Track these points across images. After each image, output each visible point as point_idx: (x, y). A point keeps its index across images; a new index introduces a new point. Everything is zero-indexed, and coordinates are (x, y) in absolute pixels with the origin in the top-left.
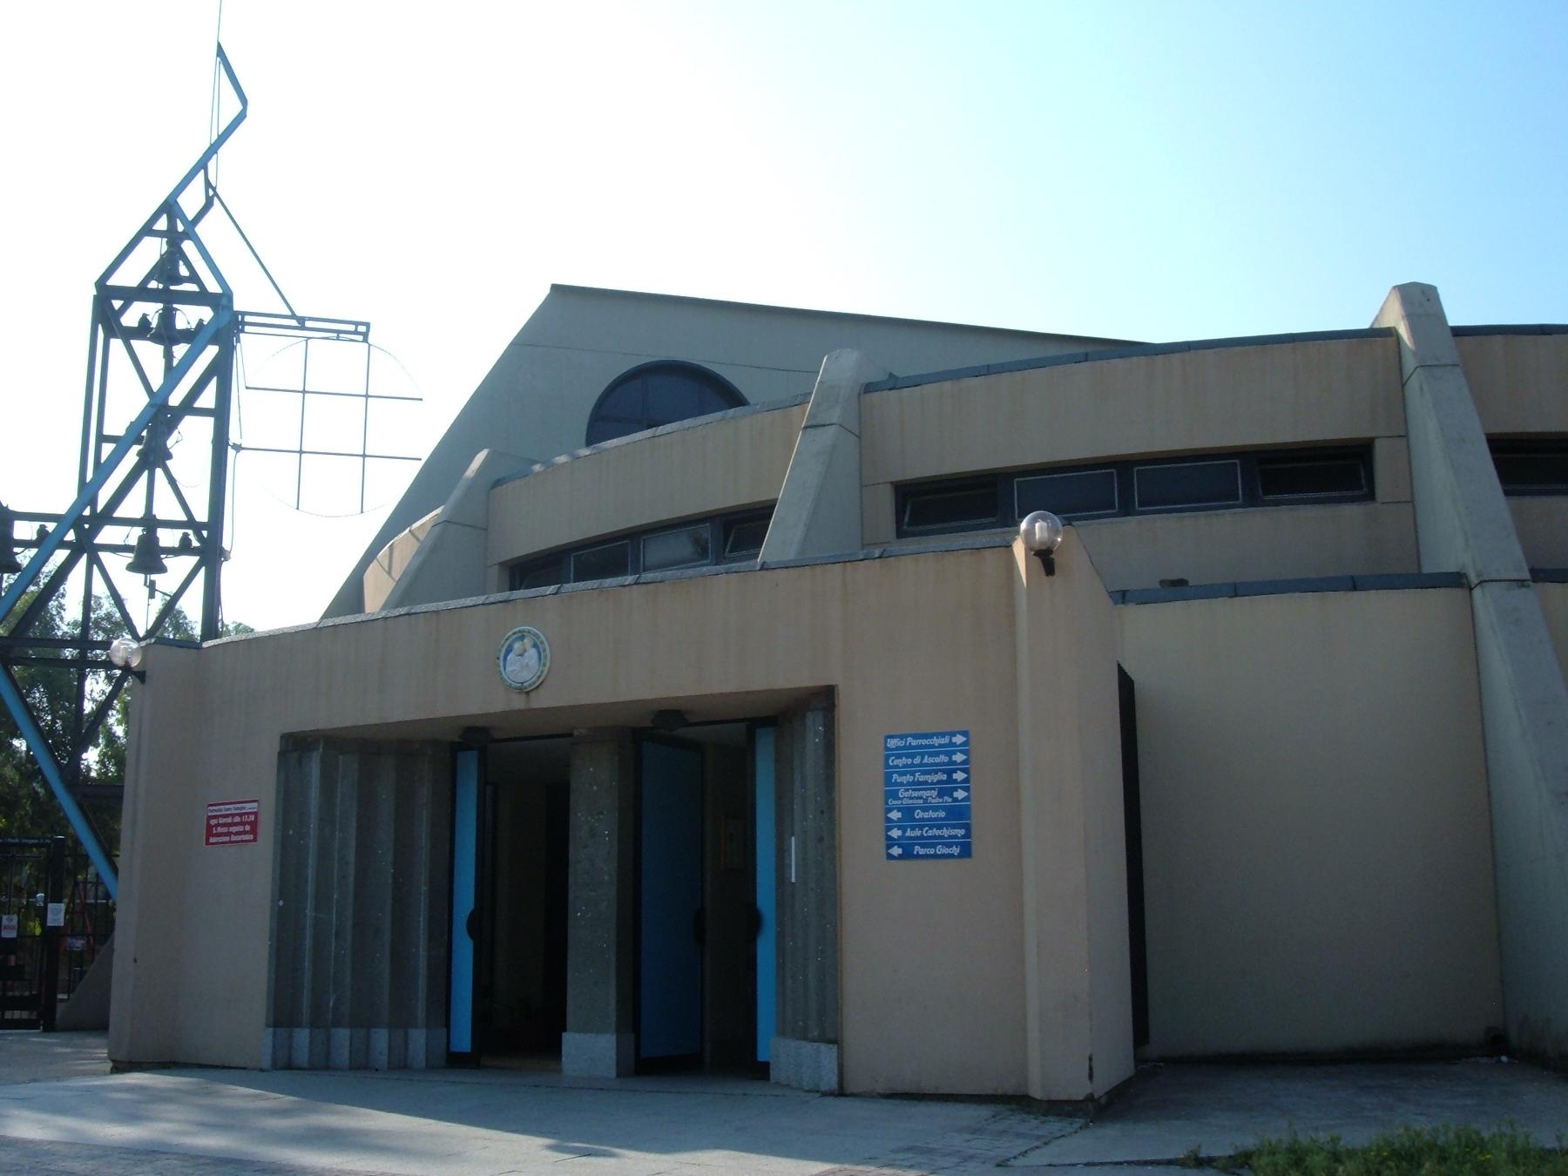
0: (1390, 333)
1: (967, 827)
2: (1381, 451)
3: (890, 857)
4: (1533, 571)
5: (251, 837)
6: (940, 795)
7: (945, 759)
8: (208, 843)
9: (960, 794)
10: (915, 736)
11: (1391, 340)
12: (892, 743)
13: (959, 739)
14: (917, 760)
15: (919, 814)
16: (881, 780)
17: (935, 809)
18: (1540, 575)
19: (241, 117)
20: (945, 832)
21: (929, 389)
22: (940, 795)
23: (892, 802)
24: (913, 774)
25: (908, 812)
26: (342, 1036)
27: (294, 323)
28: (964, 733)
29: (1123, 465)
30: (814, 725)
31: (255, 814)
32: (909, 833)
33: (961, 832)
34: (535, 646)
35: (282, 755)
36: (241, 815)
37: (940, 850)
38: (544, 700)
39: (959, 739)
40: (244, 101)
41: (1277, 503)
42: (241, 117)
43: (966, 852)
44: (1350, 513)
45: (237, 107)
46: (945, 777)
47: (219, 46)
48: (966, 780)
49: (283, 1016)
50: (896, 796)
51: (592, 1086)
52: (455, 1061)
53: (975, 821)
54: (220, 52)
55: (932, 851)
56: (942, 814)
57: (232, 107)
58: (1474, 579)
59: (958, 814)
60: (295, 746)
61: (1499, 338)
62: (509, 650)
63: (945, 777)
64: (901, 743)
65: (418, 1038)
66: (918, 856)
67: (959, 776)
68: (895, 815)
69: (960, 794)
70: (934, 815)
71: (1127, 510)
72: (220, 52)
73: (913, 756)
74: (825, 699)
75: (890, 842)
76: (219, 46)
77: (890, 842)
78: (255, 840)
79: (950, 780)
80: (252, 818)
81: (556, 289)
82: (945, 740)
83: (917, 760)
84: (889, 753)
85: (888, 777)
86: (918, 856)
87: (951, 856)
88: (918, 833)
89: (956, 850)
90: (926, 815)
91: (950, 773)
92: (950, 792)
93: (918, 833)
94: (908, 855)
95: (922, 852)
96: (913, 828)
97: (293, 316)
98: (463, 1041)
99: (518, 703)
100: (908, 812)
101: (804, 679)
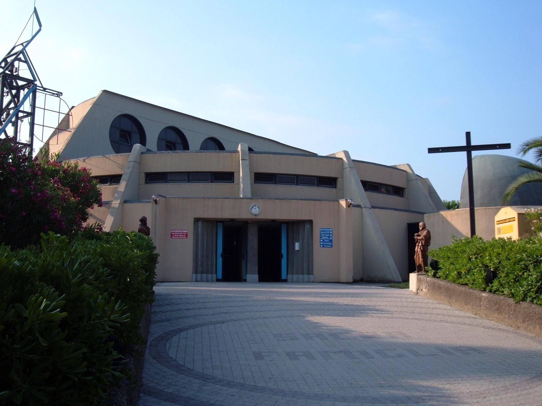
0: (341, 159)
1: (332, 243)
2: (406, 190)
3: (321, 247)
4: (371, 206)
5: (186, 237)
6: (328, 238)
7: (329, 233)
8: (171, 237)
9: (331, 238)
10: (325, 229)
11: (342, 160)
12: (321, 229)
13: (331, 230)
14: (325, 232)
15: (325, 241)
16: (320, 235)
17: (328, 240)
18: (373, 207)
19: (39, 31)
20: (329, 243)
21: (263, 155)
22: (328, 238)
23: (321, 239)
24: (324, 234)
25: (323, 240)
26: (205, 275)
27: (42, 89)
28: (332, 229)
29: (297, 176)
30: (308, 226)
31: (187, 233)
32: (324, 243)
33: (331, 244)
34: (258, 208)
35: (194, 221)
36: (182, 233)
37: (328, 246)
38: (259, 217)
39: (331, 230)
40: (40, 25)
41: (322, 187)
42: (39, 31)
43: (332, 247)
44: (334, 190)
45: (38, 28)
46: (329, 235)
47: (35, 8)
48: (332, 236)
49: (196, 271)
50: (321, 237)
51: (253, 282)
52: (218, 280)
53: (333, 242)
54: (35, 11)
55: (326, 246)
56: (328, 241)
58: (363, 206)
59: (331, 241)
60: (197, 220)
61: (357, 162)
62: (252, 208)
63: (329, 235)
64: (322, 230)
65: (214, 276)
66: (325, 247)
67: (331, 235)
68: (322, 240)
69: (331, 238)
70: (327, 241)
71: (297, 184)
72: (35, 11)
73: (324, 232)
74: (311, 222)
75: (321, 245)
76: (35, 8)
77: (321, 245)
78: (187, 238)
79: (330, 236)
80: (186, 233)
81: (105, 92)
82: (329, 230)
83: (325, 232)
84: (321, 231)
85: (320, 235)
86: (325, 247)
87: (329, 247)
88: (325, 243)
89: (330, 246)
90: (326, 241)
91: (329, 235)
92: (329, 238)
93: (325, 243)
94: (323, 246)
95: (325, 246)
96: (324, 243)
97: (42, 87)
98: (220, 276)
99: (254, 217)
100: (323, 240)
101: (307, 218)
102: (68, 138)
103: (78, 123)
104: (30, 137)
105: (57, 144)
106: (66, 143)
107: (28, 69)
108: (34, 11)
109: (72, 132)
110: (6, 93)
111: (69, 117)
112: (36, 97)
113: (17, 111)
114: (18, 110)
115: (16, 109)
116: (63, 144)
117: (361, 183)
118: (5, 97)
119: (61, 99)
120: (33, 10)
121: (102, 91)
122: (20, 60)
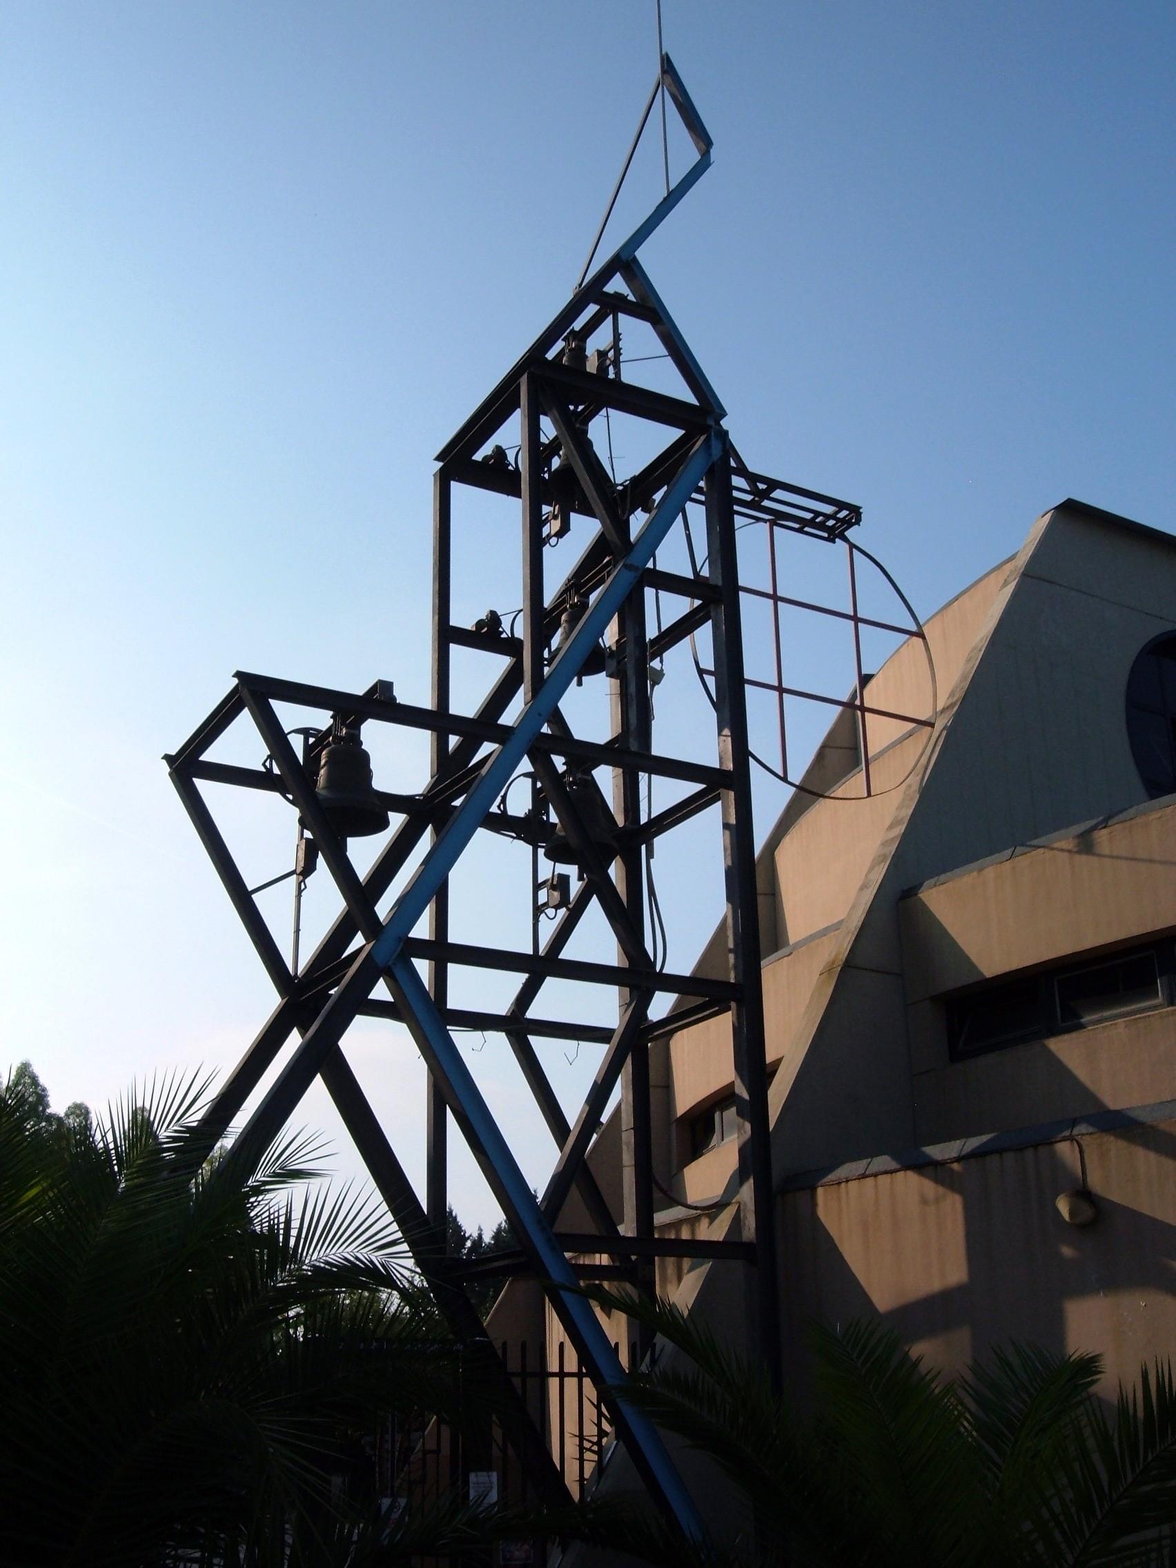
57: (686, 154)
81: (1071, 511)
102: (924, 760)
103: (963, 678)
104: (726, 732)
105: (869, 795)
106: (916, 787)
107: (663, 350)
108: (664, 72)
109: (939, 725)
110: (553, 887)
111: (854, 717)
112: (641, 800)
113: (630, 577)
114: (637, 568)
115: (625, 566)
116: (896, 797)
117: (731, 1083)
118: (553, 541)
119: (853, 546)
120: (656, 70)
121: (1049, 516)
122: (614, 305)
